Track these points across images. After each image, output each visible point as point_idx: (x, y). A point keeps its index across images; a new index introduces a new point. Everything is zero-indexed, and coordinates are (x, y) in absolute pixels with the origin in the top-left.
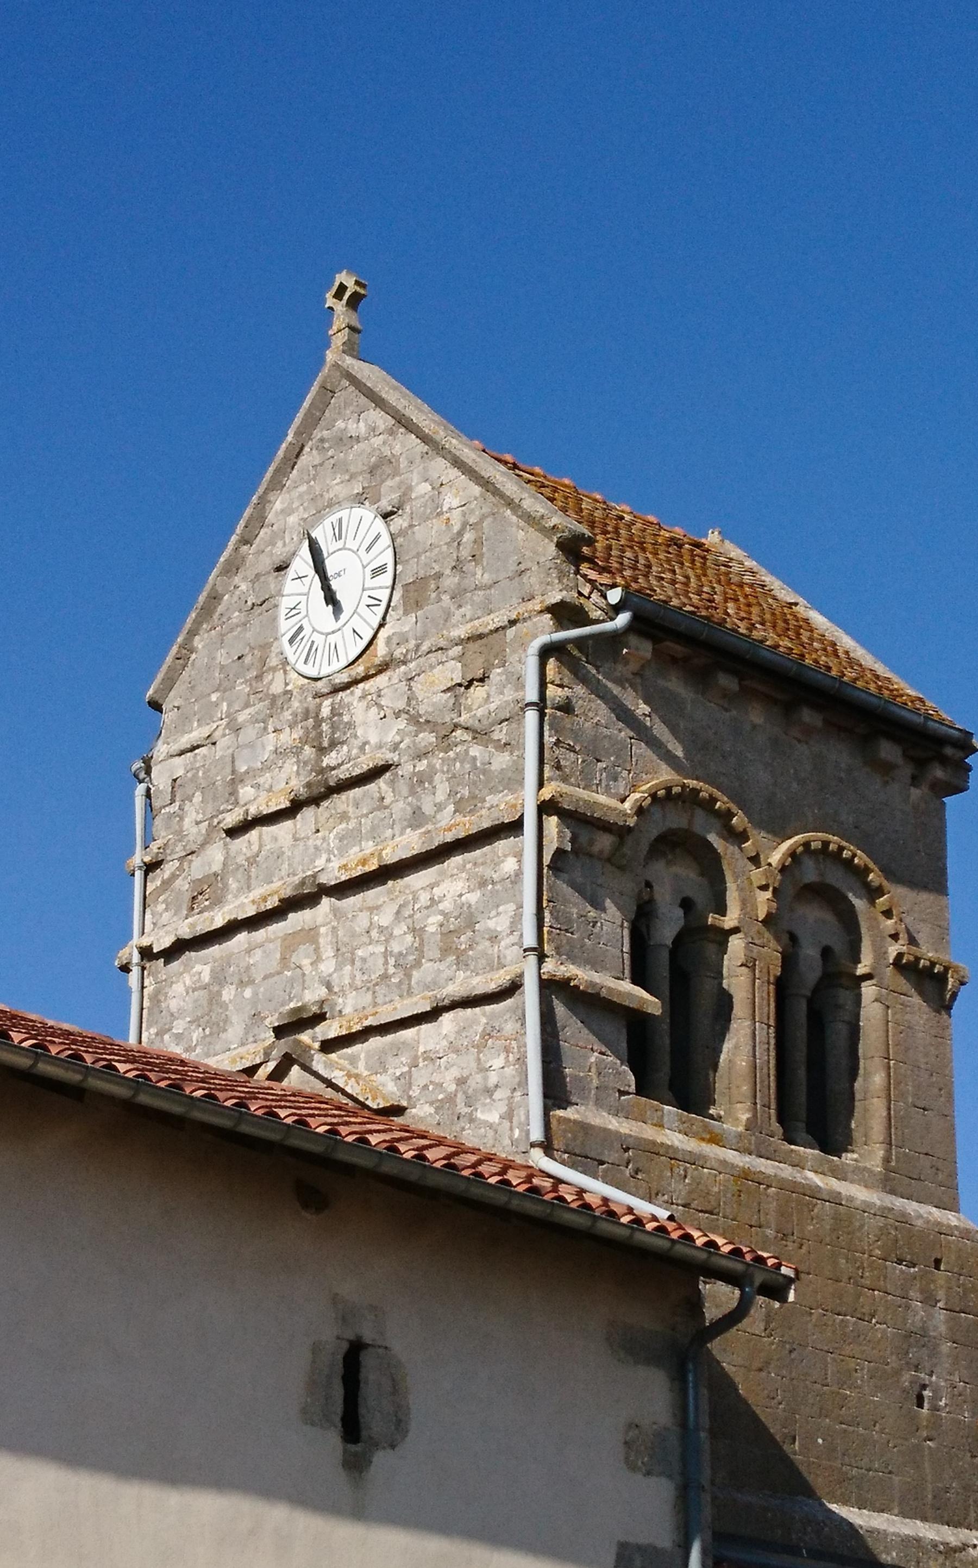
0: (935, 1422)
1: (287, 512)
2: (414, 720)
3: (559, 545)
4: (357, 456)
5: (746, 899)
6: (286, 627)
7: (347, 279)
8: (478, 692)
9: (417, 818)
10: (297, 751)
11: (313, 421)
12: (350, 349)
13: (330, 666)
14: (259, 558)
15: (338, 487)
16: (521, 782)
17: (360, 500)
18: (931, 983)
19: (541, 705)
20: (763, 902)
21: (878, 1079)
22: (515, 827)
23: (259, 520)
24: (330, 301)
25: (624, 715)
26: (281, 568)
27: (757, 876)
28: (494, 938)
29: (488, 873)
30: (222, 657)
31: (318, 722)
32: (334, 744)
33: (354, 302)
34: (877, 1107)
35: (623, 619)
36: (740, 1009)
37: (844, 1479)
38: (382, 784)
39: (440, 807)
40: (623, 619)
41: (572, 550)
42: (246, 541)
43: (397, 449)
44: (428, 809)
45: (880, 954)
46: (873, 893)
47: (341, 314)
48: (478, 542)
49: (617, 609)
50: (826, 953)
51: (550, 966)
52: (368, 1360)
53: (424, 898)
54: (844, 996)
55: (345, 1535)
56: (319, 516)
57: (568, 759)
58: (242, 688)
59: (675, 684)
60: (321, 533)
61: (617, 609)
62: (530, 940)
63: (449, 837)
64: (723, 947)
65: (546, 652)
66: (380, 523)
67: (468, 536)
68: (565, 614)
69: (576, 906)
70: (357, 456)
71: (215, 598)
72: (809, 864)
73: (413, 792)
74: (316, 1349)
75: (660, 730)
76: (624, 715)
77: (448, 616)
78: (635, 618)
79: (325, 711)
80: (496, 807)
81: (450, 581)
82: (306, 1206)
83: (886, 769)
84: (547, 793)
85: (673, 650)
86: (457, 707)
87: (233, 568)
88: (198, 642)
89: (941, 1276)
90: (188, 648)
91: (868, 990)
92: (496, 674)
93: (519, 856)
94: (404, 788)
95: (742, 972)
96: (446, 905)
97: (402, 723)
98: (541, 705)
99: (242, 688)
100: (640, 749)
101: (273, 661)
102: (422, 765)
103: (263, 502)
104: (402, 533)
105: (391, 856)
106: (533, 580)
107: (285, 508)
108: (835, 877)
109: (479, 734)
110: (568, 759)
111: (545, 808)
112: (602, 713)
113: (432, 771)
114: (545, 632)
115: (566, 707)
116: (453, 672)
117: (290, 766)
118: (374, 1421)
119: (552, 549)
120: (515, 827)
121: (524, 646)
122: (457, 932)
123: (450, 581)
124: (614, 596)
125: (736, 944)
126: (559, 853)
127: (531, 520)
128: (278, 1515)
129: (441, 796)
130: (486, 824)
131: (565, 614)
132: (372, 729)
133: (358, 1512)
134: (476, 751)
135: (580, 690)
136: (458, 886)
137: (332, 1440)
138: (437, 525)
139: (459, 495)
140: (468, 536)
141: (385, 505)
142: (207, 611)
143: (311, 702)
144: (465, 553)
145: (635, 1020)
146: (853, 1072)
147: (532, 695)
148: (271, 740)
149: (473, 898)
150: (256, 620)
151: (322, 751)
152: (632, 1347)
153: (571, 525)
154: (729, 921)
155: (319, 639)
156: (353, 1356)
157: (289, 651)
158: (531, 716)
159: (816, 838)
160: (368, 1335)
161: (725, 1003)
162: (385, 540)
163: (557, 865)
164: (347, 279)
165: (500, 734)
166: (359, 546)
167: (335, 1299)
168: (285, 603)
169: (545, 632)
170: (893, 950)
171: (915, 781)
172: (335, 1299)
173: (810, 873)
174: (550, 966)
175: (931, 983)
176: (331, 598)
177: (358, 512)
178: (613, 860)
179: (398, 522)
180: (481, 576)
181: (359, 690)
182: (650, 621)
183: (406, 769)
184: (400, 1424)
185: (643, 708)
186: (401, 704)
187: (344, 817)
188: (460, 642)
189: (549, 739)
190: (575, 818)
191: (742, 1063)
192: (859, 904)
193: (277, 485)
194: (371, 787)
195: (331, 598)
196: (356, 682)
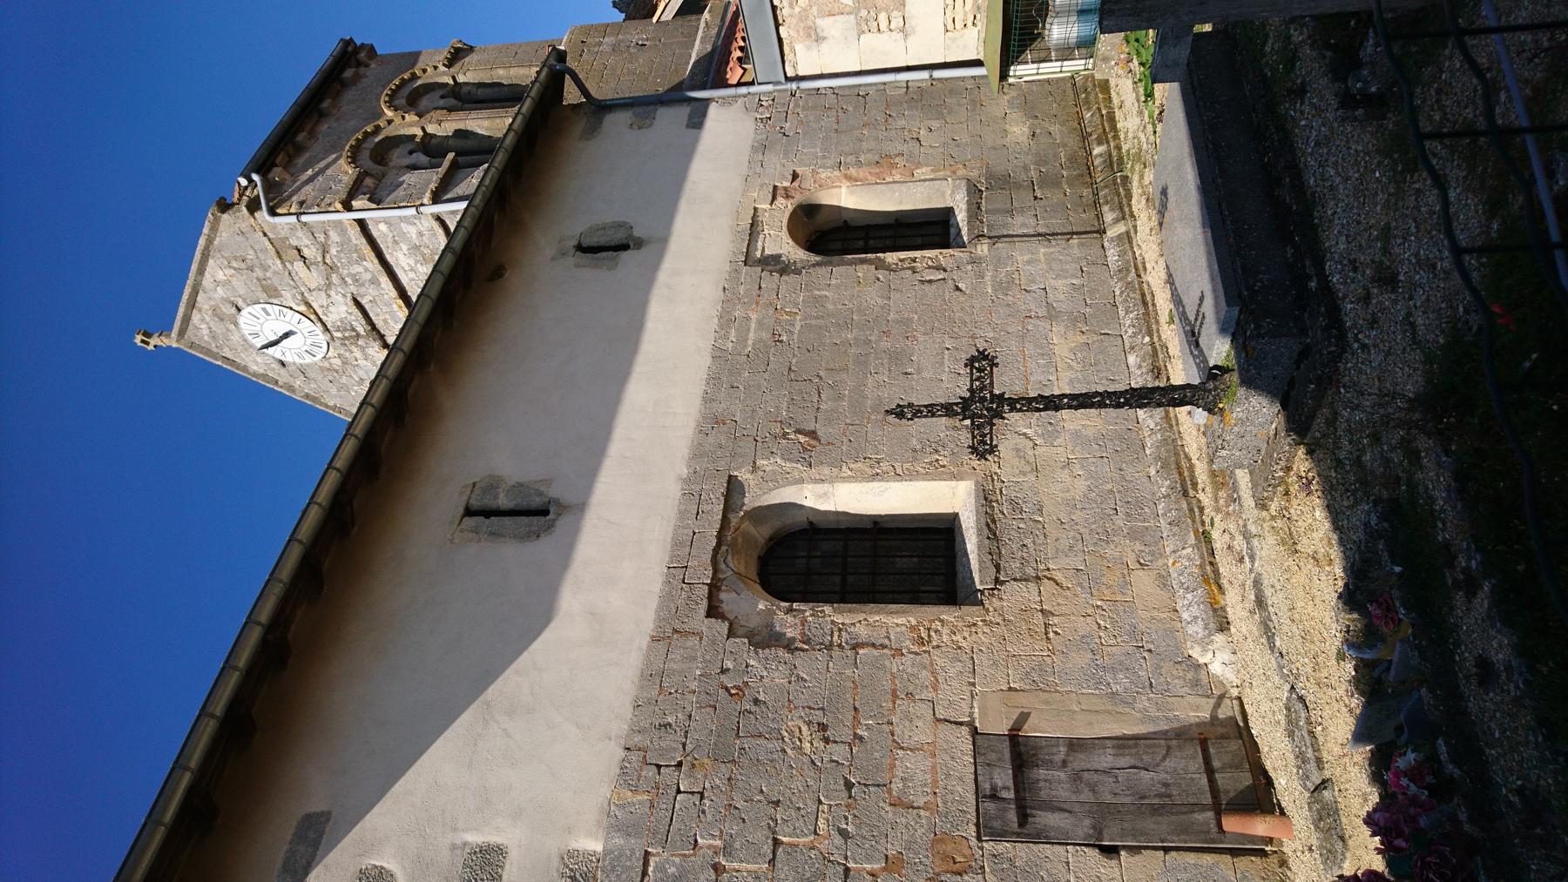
0: (653, 39)
1: (256, 363)
2: (329, 285)
3: (223, 212)
4: (219, 328)
5: (409, 125)
6: (308, 359)
7: (138, 339)
8: (306, 252)
9: (374, 281)
10: (362, 349)
11: (208, 352)
12: (168, 336)
13: (322, 338)
14: (282, 376)
15: (235, 338)
16: (340, 222)
17: (236, 324)
18: (457, 56)
19: (298, 215)
20: (411, 118)
21: (501, 72)
22: (362, 224)
23: (264, 376)
24: (151, 348)
25: (311, 179)
26: (283, 364)
27: (398, 120)
28: (420, 234)
29: (390, 239)
30: (334, 391)
31: (345, 338)
32: (353, 330)
33: (148, 335)
34: (513, 71)
35: (255, 177)
36: (461, 126)
37: (676, 71)
38: (363, 301)
39: (366, 270)
40: (255, 177)
41: (225, 206)
42: (276, 382)
43: (206, 307)
44: (368, 276)
45: (444, 73)
46: (414, 77)
47: (154, 341)
48: (236, 259)
49: (251, 181)
50: (442, 97)
51: (426, 201)
52: (586, 242)
53: (412, 275)
54: (465, 89)
55: (674, 245)
56: (251, 346)
57: (327, 200)
58: (344, 380)
59: (301, 161)
60: (259, 343)
61: (251, 181)
62: (412, 211)
63: (376, 261)
64: (433, 136)
65: (272, 212)
66: (244, 313)
67: (235, 264)
68: (253, 206)
69: (400, 192)
70: (219, 328)
71: (307, 396)
72: (396, 102)
73: (362, 285)
74: (577, 266)
75: (322, 164)
76: (311, 179)
77: (275, 273)
78: (257, 172)
79: (339, 335)
80: (355, 234)
81: (259, 273)
82: (501, 276)
83: (357, 78)
84: (339, 206)
85: (280, 160)
86: (316, 264)
87: (291, 388)
88: (331, 404)
89: (590, 40)
90: (334, 408)
91: (461, 79)
92: (294, 242)
93: (377, 221)
94: (363, 290)
95: (443, 126)
96: (412, 262)
97: (332, 293)
98: (298, 215)
99: (344, 380)
100: (329, 172)
101: (326, 364)
102: (349, 280)
103: (255, 375)
104: (244, 300)
105: (393, 293)
106: (244, 226)
107: (257, 364)
108: (406, 91)
109: (325, 252)
110: (327, 200)
111: (348, 207)
112: (308, 188)
113: (349, 275)
114: (263, 215)
115: (301, 203)
116: (299, 265)
117: (370, 351)
118: (618, 237)
119: (225, 216)
120: (362, 224)
121: (274, 227)
122: (423, 255)
123: (259, 273)
124: (244, 182)
125: (431, 129)
126: (370, 200)
127: (214, 229)
128: (663, 276)
129: (361, 269)
130: (364, 241)
131: (253, 206)
132: (339, 311)
133: (664, 241)
134: (333, 251)
135: (295, 198)
136: (400, 256)
137: (624, 255)
138: (234, 282)
139: (216, 272)
140: (235, 264)
141: (234, 310)
142: (314, 399)
143: (338, 343)
144: (243, 266)
145: (454, 166)
146: (500, 85)
147: (293, 219)
148: (362, 362)
149: (405, 248)
150: (311, 374)
151: (358, 335)
152: (592, 130)
153: (213, 209)
154: (420, 133)
155: (309, 342)
156: (581, 248)
157: (319, 356)
158: (304, 218)
159: (384, 98)
160: (575, 242)
161: (459, 133)
162: (250, 309)
163: (377, 200)
164: (138, 339)
165: (321, 238)
166: (259, 322)
167: (553, 259)
168: (298, 361)
169: (263, 215)
170: (442, 68)
171: (367, 66)
172: (553, 259)
173: (401, 101)
174: (426, 201)
175: (457, 56)
176: (286, 335)
177: (242, 325)
178: (380, 178)
179: (240, 303)
180: (251, 255)
181: (324, 318)
182: (263, 164)
183: (353, 289)
184: (620, 225)
185: (310, 172)
186: (323, 294)
187: (385, 321)
188: (283, 263)
189: (316, 209)
190: (353, 193)
191: (486, 123)
192: (419, 82)
193: (245, 369)
194: (367, 307)
195: (286, 335)
196: (320, 320)
